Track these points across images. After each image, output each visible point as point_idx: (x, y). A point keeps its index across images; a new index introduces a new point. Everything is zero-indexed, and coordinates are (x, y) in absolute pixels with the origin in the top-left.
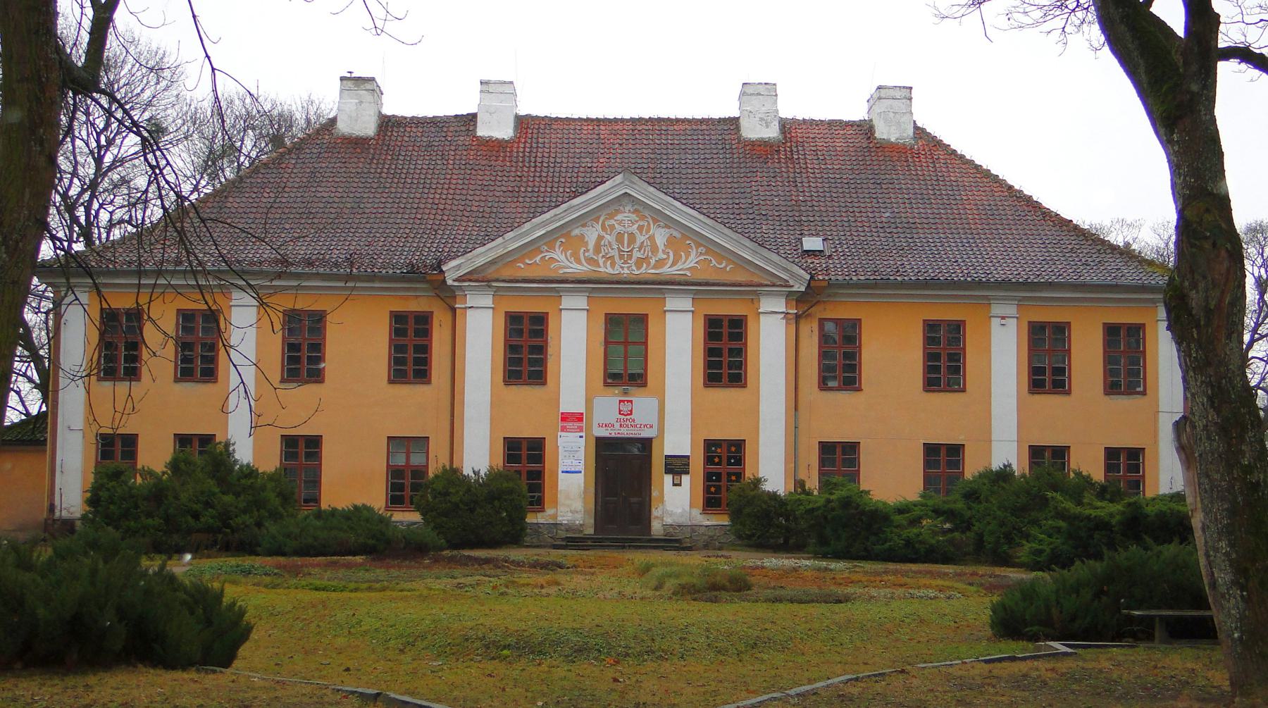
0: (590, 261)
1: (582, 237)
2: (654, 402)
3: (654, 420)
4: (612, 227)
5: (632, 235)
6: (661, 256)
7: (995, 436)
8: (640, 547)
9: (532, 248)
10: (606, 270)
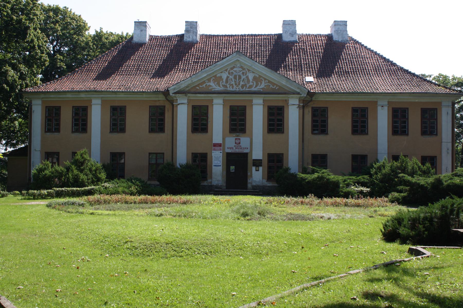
0: (223, 86)
1: (221, 77)
6: (251, 84)
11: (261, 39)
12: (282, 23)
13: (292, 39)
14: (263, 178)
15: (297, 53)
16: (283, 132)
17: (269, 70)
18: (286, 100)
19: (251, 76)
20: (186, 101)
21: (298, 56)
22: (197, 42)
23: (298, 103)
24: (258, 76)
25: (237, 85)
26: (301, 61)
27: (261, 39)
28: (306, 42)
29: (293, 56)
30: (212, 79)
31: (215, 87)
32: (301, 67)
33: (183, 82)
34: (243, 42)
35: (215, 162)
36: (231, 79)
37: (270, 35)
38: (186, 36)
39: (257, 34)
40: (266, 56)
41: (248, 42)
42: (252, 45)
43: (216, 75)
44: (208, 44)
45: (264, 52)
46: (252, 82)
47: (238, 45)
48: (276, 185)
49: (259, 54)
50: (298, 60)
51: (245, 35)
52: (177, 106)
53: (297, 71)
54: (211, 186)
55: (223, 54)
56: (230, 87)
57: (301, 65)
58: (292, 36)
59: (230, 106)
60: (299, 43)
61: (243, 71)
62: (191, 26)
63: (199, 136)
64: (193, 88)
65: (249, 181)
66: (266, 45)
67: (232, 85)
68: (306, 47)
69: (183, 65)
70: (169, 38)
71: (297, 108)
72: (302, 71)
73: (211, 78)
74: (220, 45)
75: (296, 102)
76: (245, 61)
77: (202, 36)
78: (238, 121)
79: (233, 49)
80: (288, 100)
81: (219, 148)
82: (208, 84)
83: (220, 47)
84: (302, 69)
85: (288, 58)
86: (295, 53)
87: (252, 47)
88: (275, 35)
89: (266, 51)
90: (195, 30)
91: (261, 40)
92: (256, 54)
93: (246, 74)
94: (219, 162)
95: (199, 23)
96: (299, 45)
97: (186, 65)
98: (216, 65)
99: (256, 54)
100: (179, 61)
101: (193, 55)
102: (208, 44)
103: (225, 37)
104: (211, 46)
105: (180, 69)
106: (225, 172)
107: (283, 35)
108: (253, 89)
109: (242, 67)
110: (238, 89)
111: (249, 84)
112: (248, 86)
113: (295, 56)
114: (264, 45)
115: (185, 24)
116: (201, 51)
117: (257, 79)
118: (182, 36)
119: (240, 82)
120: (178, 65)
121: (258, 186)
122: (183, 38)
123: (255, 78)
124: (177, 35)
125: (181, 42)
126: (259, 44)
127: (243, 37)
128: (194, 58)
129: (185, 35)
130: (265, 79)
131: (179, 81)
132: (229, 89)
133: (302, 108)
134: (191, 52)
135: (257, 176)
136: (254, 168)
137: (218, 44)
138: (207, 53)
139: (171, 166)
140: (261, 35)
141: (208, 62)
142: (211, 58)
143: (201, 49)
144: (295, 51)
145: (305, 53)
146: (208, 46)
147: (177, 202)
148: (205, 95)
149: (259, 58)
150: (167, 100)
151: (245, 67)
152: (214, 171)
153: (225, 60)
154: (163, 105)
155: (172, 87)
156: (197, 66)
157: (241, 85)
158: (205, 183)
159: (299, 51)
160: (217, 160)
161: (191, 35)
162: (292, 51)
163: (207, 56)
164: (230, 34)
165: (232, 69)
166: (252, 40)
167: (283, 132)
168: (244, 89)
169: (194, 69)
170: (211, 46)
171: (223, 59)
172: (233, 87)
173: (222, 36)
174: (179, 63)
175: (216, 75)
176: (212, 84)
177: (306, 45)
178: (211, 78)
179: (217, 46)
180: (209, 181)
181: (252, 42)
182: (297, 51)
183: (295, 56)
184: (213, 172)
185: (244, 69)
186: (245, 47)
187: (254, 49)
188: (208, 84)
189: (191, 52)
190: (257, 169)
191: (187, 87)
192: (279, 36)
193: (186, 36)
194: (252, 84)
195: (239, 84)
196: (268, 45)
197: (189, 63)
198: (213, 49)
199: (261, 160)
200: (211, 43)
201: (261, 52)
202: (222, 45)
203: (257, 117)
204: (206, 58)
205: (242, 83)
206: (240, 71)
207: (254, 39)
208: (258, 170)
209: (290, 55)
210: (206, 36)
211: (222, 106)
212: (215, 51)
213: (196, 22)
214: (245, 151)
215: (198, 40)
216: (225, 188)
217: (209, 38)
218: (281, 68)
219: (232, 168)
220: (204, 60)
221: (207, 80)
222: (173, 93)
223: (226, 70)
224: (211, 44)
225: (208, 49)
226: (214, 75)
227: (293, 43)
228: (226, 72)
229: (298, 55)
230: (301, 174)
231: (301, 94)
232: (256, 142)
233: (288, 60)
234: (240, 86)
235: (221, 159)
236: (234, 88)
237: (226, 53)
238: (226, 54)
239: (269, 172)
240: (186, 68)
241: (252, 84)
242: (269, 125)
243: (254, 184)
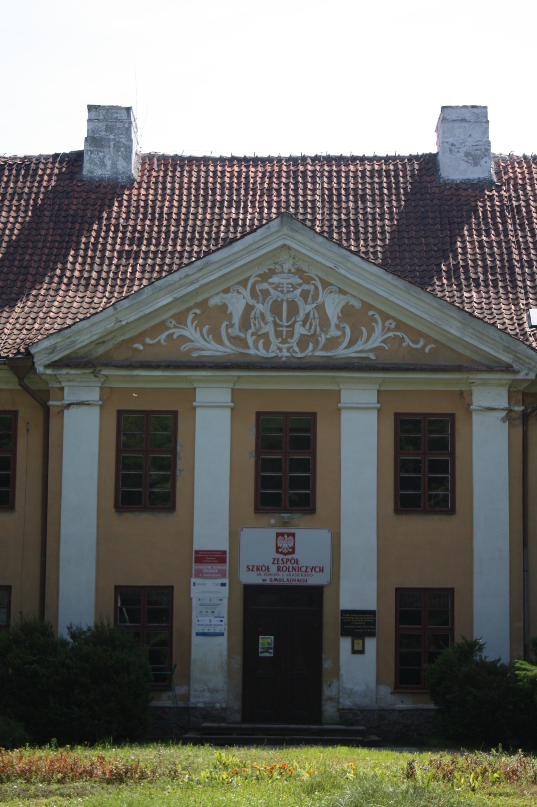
0: (233, 339)
1: (224, 307)
6: (333, 332)
11: (363, 172)
12: (437, 113)
13: (474, 174)
14: (379, 682)
15: (495, 224)
16: (452, 511)
17: (399, 283)
18: (461, 393)
19: (333, 306)
20: (94, 395)
21: (497, 235)
22: (130, 183)
23: (504, 404)
24: (358, 305)
25: (284, 337)
26: (510, 253)
27: (363, 172)
28: (524, 186)
29: (479, 235)
30: (191, 316)
31: (201, 343)
32: (512, 274)
33: (85, 323)
34: (296, 184)
35: (200, 621)
36: (262, 315)
37: (394, 158)
38: (91, 161)
39: (347, 154)
40: (383, 232)
41: (314, 183)
42: (330, 195)
43: (206, 300)
44: (173, 189)
45: (374, 220)
46: (337, 327)
47: (279, 195)
48: (432, 706)
49: (356, 226)
50: (500, 247)
51: (304, 159)
52: (61, 413)
53: (495, 286)
54: (187, 709)
55: (227, 226)
56: (256, 342)
57: (512, 267)
58: (476, 163)
59: (259, 414)
60: (499, 189)
61: (306, 287)
62: (110, 123)
63: (143, 524)
64: (120, 345)
65: (328, 692)
66: (381, 194)
67: (266, 336)
68: (527, 201)
69: (83, 264)
70: (28, 167)
71: (503, 420)
72: (515, 287)
73: (188, 310)
74: (214, 194)
75: (501, 400)
76: (312, 249)
77: (148, 159)
78: (286, 469)
79: (261, 208)
80: (471, 393)
81: (218, 567)
82: (177, 332)
83: (214, 201)
84: (513, 281)
85: (463, 242)
86: (487, 224)
87: (331, 202)
88: (411, 158)
89: (382, 215)
90: (123, 140)
91: (363, 177)
92: (348, 227)
93: (315, 298)
94: (215, 621)
95: (139, 116)
96: (500, 196)
97: (92, 265)
98: (207, 264)
99: (348, 227)
100: (68, 250)
101: (117, 226)
102: (173, 189)
103: (232, 166)
104: (180, 195)
105: (70, 278)
106: (238, 659)
107: (440, 158)
108: (342, 352)
109: (299, 272)
110: (285, 353)
111: (326, 332)
112: (322, 340)
113: (488, 235)
114: (373, 195)
115: (85, 115)
116: (145, 214)
117: (357, 317)
118: (75, 159)
119: (292, 326)
120: (65, 263)
121: (362, 711)
122: (81, 167)
123: (347, 313)
124: (56, 156)
125: (71, 179)
126: (355, 190)
127: (296, 165)
128: (123, 239)
129: (86, 157)
130: (386, 317)
131: (69, 322)
132: (252, 351)
133: (519, 422)
134: (109, 219)
135: (358, 672)
136: (345, 644)
137: (206, 189)
138: (169, 220)
139: (39, 633)
140: (363, 159)
141: (172, 253)
142: (183, 239)
143: (145, 207)
144: (485, 218)
145: (522, 225)
146: (172, 195)
147: (90, 774)
148: (167, 373)
149: (357, 240)
150: (26, 388)
151: (313, 273)
152: (195, 654)
153: (237, 246)
154: (9, 408)
155: (46, 344)
156: (134, 267)
157: (296, 337)
158: (164, 701)
159: (503, 216)
160: (209, 613)
161: (108, 156)
162: (477, 218)
163: (167, 233)
164: (250, 154)
165: (264, 277)
166: (330, 177)
167: (452, 511)
168: (308, 352)
169: (123, 280)
170: (180, 195)
171: (229, 242)
172: (267, 345)
173: (222, 159)
174: (67, 255)
175: (206, 300)
176: (189, 331)
177: (525, 195)
178: (188, 310)
179: (205, 196)
180: (180, 690)
181: (330, 182)
182: (494, 218)
183: (488, 235)
184: (193, 657)
185: (308, 280)
186: (304, 203)
187: (339, 209)
188: (177, 332)
189: (109, 219)
190: (358, 647)
191: (100, 342)
192: (428, 163)
193: (91, 161)
194: (339, 333)
195: (291, 334)
196: (389, 196)
197: (102, 258)
198: (188, 208)
199: (372, 613)
200: (181, 184)
201: (365, 221)
202: (222, 195)
203: (358, 452)
204: (167, 239)
205: (300, 330)
206: (295, 288)
207: (338, 172)
208: (362, 652)
209: (470, 230)
210: (164, 159)
211: (228, 412)
212: (196, 214)
213: (128, 110)
214: (315, 579)
215: (135, 173)
216: (238, 717)
217: (174, 166)
218: (440, 279)
219: (266, 642)
220: (157, 245)
221: (173, 317)
222: (48, 366)
223: (244, 283)
224: (181, 188)
225: (171, 207)
226: (200, 299)
227: (479, 187)
228: (242, 289)
229: (497, 230)
230: (528, 666)
231: (516, 372)
232: (353, 545)
233: (464, 248)
234: (294, 341)
235: (223, 609)
236: (273, 347)
237: (236, 220)
238: (236, 225)
239: (402, 659)
240: (94, 275)
241: (339, 333)
242: (401, 483)
243: (347, 703)
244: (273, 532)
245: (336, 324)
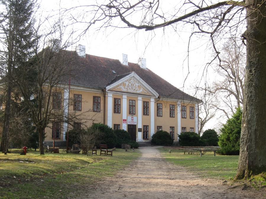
0: (127, 89)
1: (125, 84)
2: (136, 117)
3: (136, 121)
4: (130, 82)
5: (133, 84)
6: (137, 89)
7: (178, 125)
8: (145, 146)
9: (118, 86)
10: (129, 91)
176: (122, 87)
244: (131, 117)
245: (5, 154)
